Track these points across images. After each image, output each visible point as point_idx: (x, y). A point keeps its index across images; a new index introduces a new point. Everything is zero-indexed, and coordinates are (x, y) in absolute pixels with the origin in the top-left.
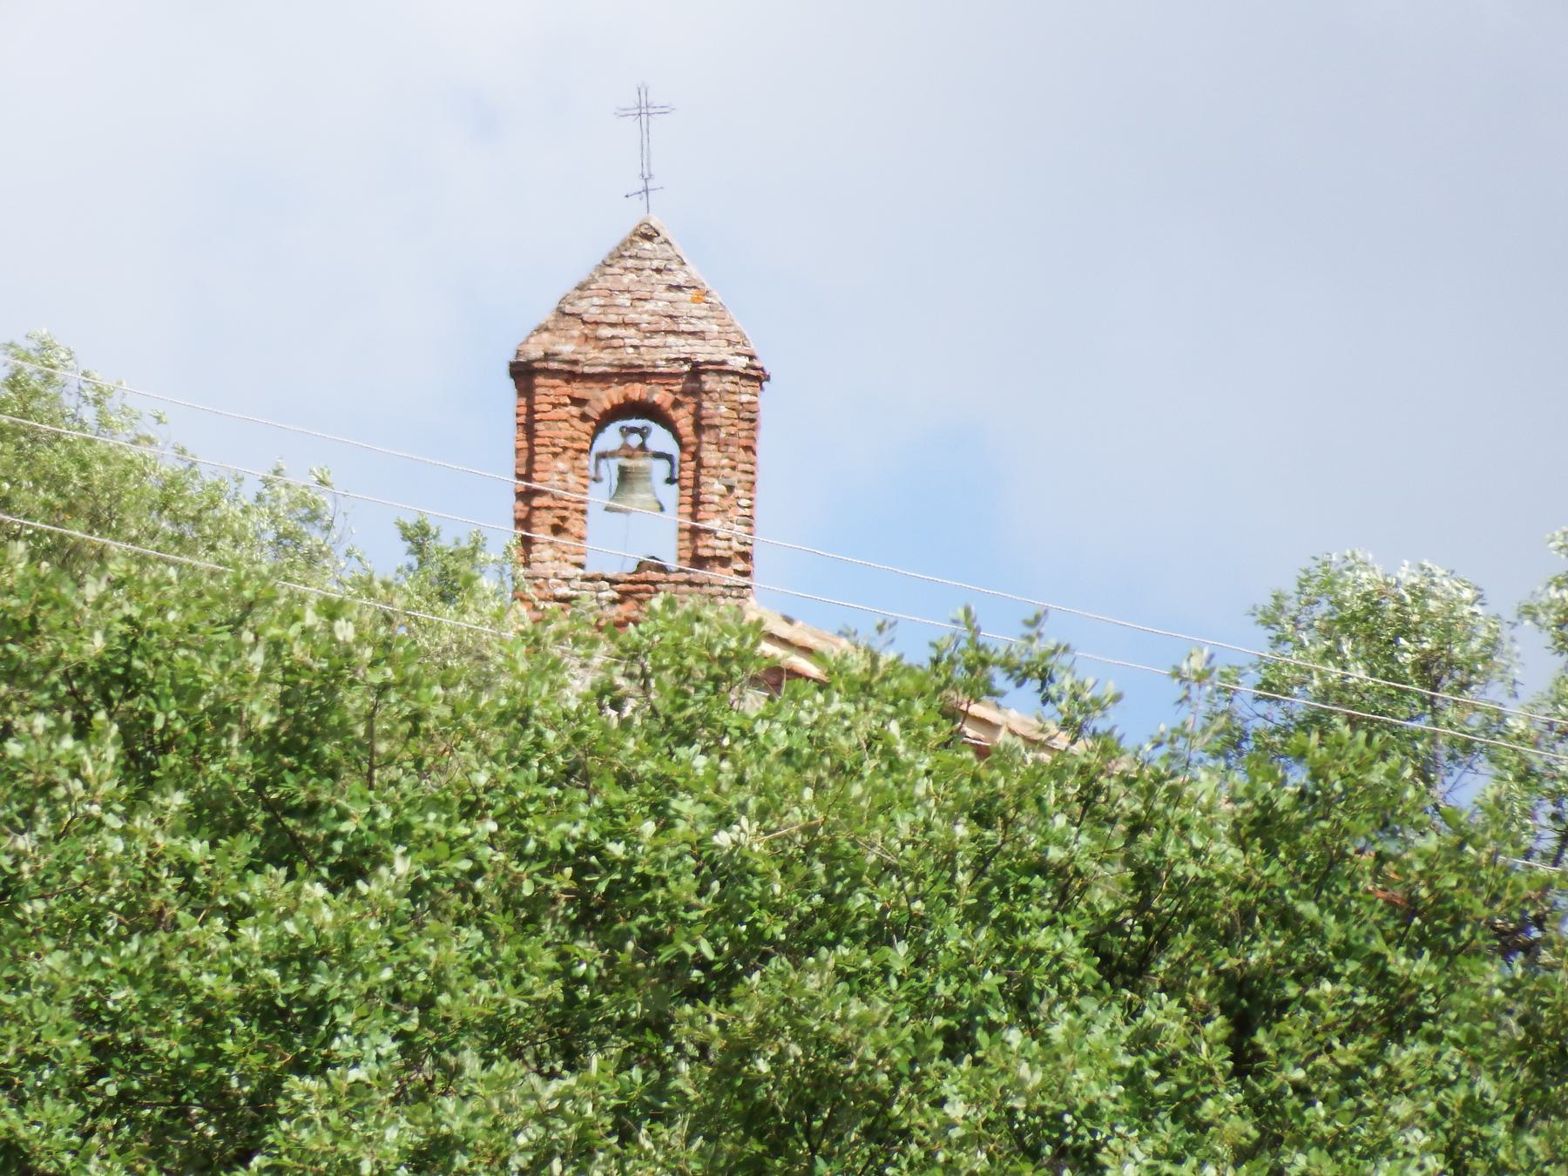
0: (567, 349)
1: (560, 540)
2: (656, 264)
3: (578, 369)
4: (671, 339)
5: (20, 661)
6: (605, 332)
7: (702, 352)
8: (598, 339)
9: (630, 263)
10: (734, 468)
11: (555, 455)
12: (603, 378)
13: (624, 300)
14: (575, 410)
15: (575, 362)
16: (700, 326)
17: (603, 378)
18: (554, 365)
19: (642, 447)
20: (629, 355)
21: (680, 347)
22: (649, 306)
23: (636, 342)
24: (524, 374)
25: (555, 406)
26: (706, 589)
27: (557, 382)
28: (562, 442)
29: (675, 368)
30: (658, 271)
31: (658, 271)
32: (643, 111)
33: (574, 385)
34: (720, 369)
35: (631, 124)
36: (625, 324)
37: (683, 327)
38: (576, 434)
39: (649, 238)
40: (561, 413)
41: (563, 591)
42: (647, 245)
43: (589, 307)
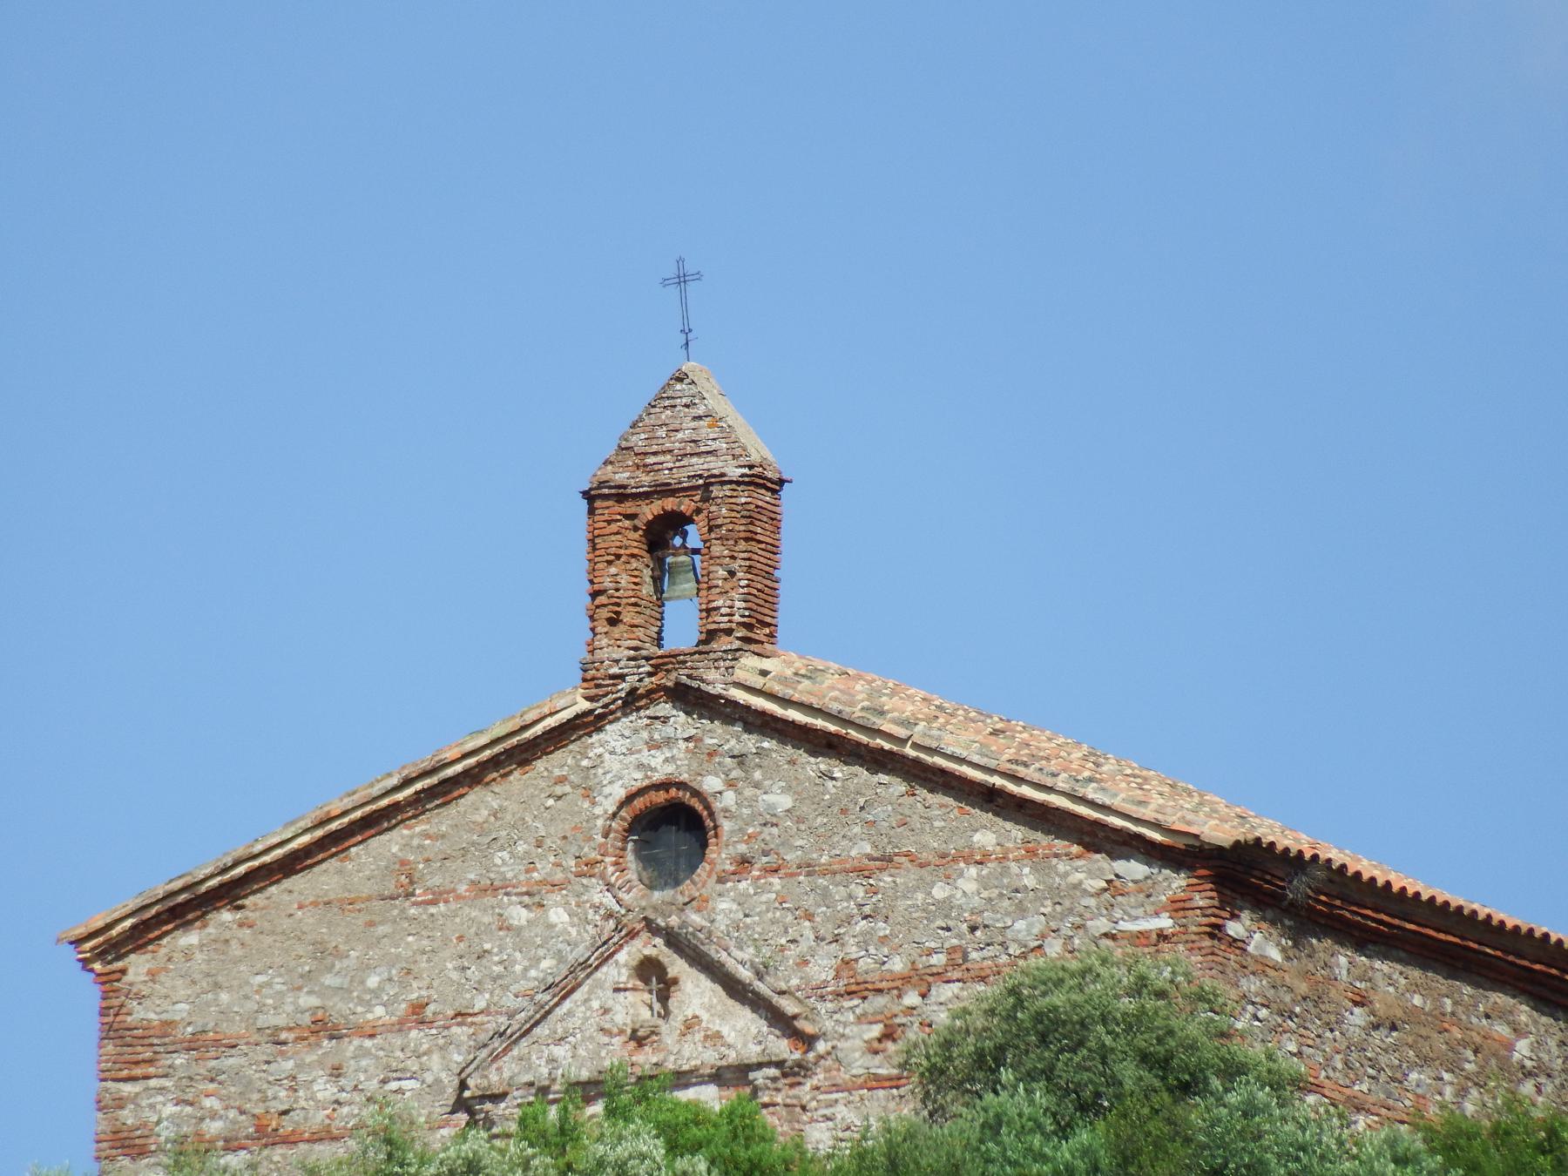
0: (622, 477)
1: (617, 631)
2: (684, 400)
3: (629, 491)
4: (694, 460)
5: (637, 852)
6: (651, 460)
7: (715, 465)
8: (645, 466)
9: (667, 403)
10: (733, 557)
11: (610, 563)
12: (646, 496)
13: (662, 432)
14: (627, 523)
15: (625, 487)
16: (714, 445)
17: (646, 496)
18: (606, 491)
19: (684, 546)
20: (664, 477)
21: (698, 465)
22: (680, 435)
23: (670, 465)
24: (589, 496)
25: (609, 522)
26: (712, 656)
27: (610, 503)
28: (613, 550)
29: (694, 482)
30: (687, 406)
31: (687, 406)
32: (682, 280)
33: (628, 504)
34: (722, 480)
35: (674, 291)
36: (664, 452)
37: (703, 449)
38: (626, 542)
39: (680, 380)
40: (614, 527)
41: (615, 670)
42: (679, 386)
43: (638, 441)
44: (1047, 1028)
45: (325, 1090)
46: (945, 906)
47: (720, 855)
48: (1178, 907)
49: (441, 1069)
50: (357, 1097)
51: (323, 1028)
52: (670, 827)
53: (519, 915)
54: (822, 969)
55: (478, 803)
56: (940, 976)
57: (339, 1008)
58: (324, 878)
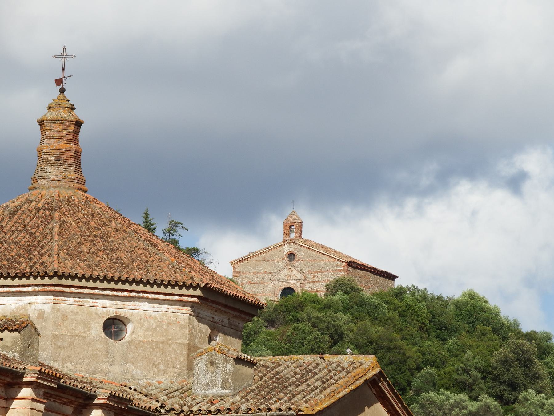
24: (41, 123)
44: (340, 285)
45: (256, 279)
46: (320, 265)
47: (297, 258)
48: (343, 267)
49: (268, 278)
50: (344, 373)
51: (256, 273)
52: (291, 256)
53: (276, 263)
54: (307, 270)
55: (272, 252)
56: (319, 272)
57: (258, 271)
58: (256, 258)
